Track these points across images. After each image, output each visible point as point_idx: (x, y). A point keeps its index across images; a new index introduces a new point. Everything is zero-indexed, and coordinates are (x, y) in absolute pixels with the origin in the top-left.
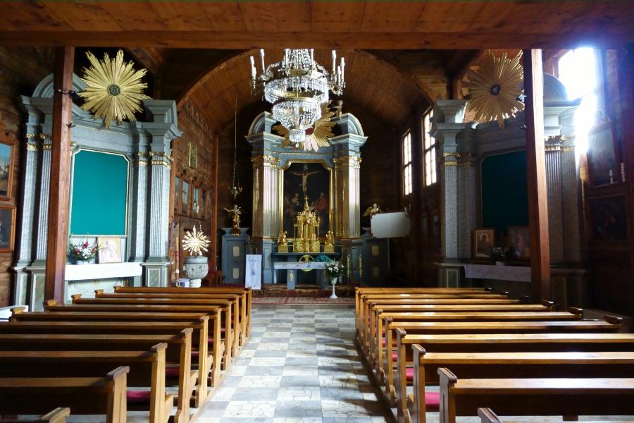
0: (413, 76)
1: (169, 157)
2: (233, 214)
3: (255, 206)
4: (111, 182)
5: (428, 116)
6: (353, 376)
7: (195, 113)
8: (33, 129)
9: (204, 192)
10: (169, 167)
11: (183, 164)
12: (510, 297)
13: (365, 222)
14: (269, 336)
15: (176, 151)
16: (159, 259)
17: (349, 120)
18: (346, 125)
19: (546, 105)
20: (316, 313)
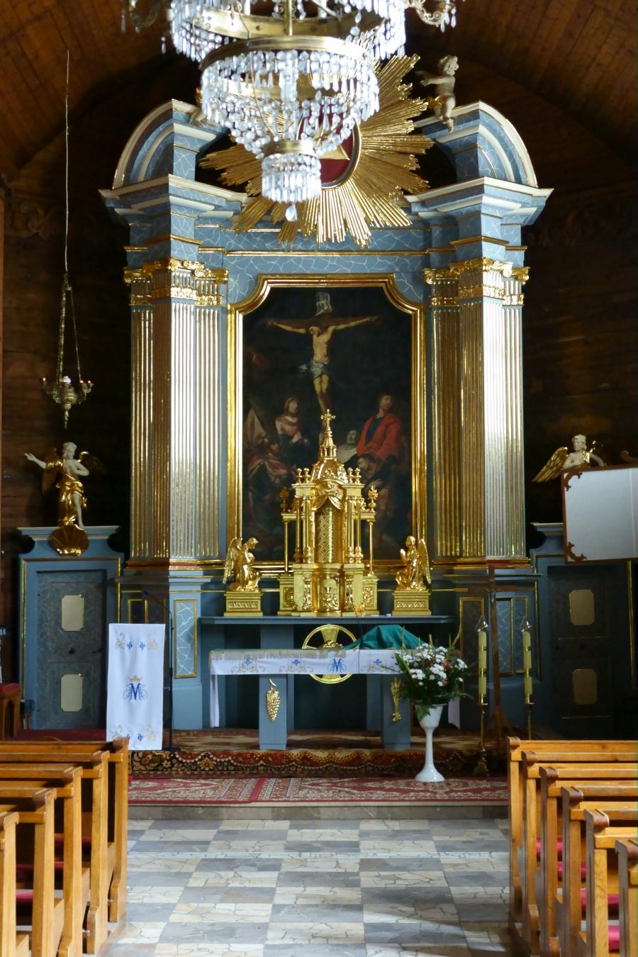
18: (471, 147)
20: (364, 835)
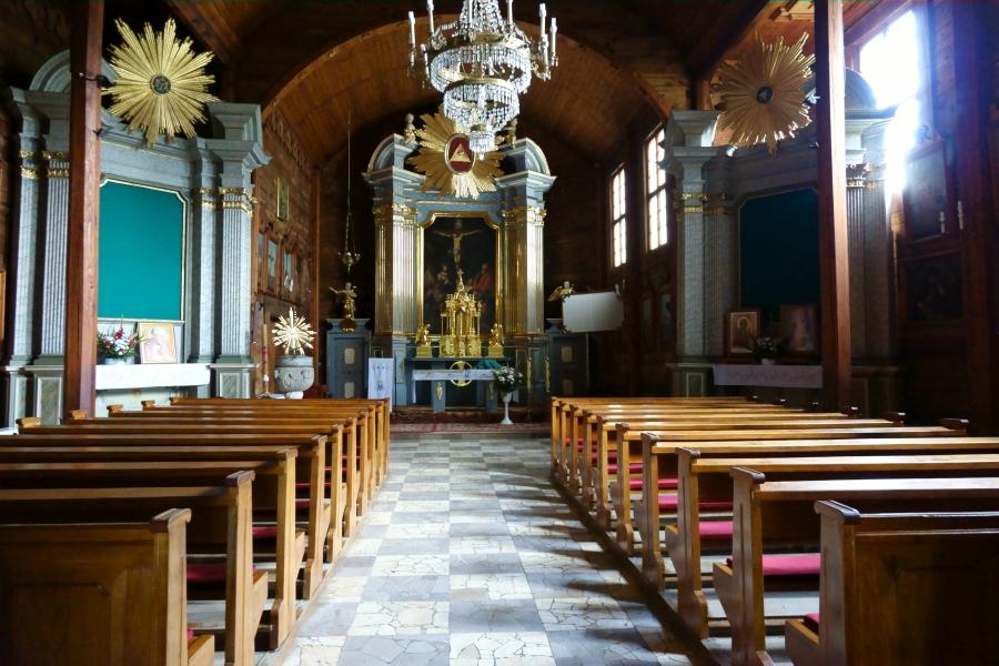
0: (635, 74)
2: (344, 297)
3: (380, 288)
4: (162, 224)
5: (654, 140)
7: (285, 132)
8: (30, 144)
9: (299, 260)
10: (250, 213)
11: (268, 213)
12: (786, 405)
13: (552, 309)
14: (417, 474)
15: (259, 191)
16: (237, 358)
17: (527, 150)
18: (522, 158)
19: (849, 116)
20: (483, 444)
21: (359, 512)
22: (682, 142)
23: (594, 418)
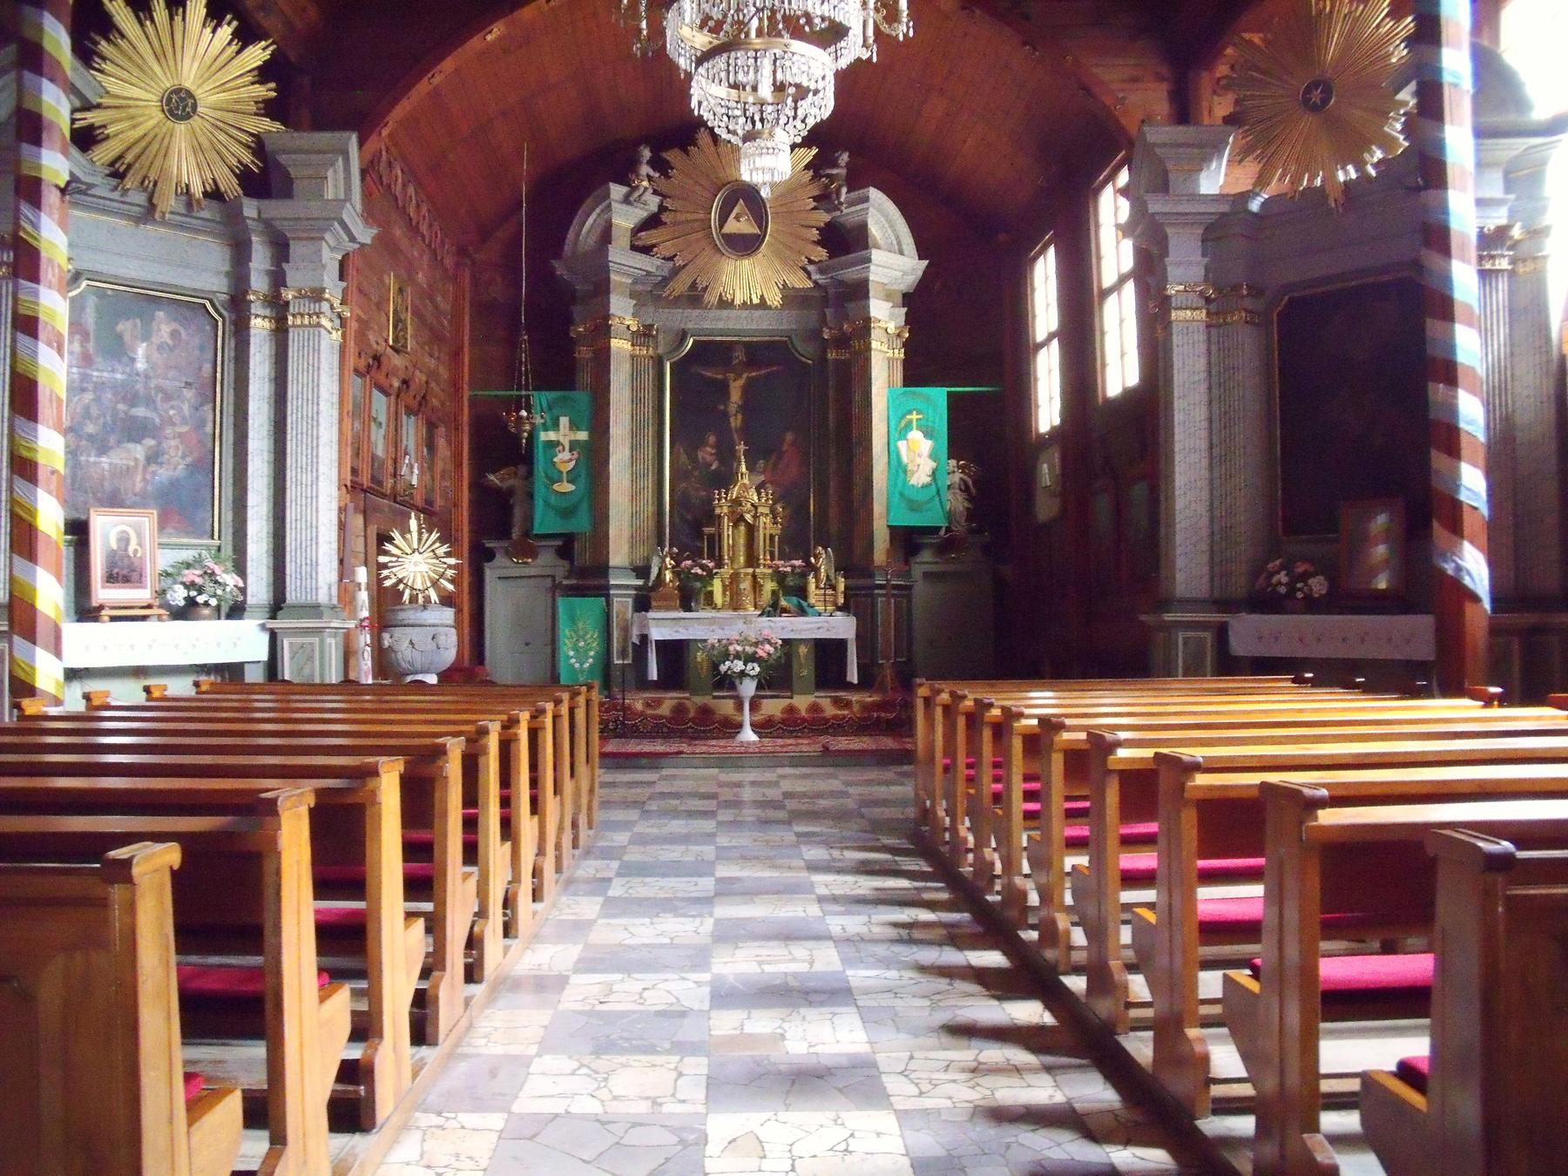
1: (337, 303)
6: (925, 916)
9: (431, 426)
10: (337, 336)
11: (372, 337)
14: (655, 831)
15: (354, 297)
16: (314, 610)
18: (863, 229)
19: (1480, 133)
20: (783, 777)
21: (537, 895)
22: (1162, 185)
23: (996, 712)
